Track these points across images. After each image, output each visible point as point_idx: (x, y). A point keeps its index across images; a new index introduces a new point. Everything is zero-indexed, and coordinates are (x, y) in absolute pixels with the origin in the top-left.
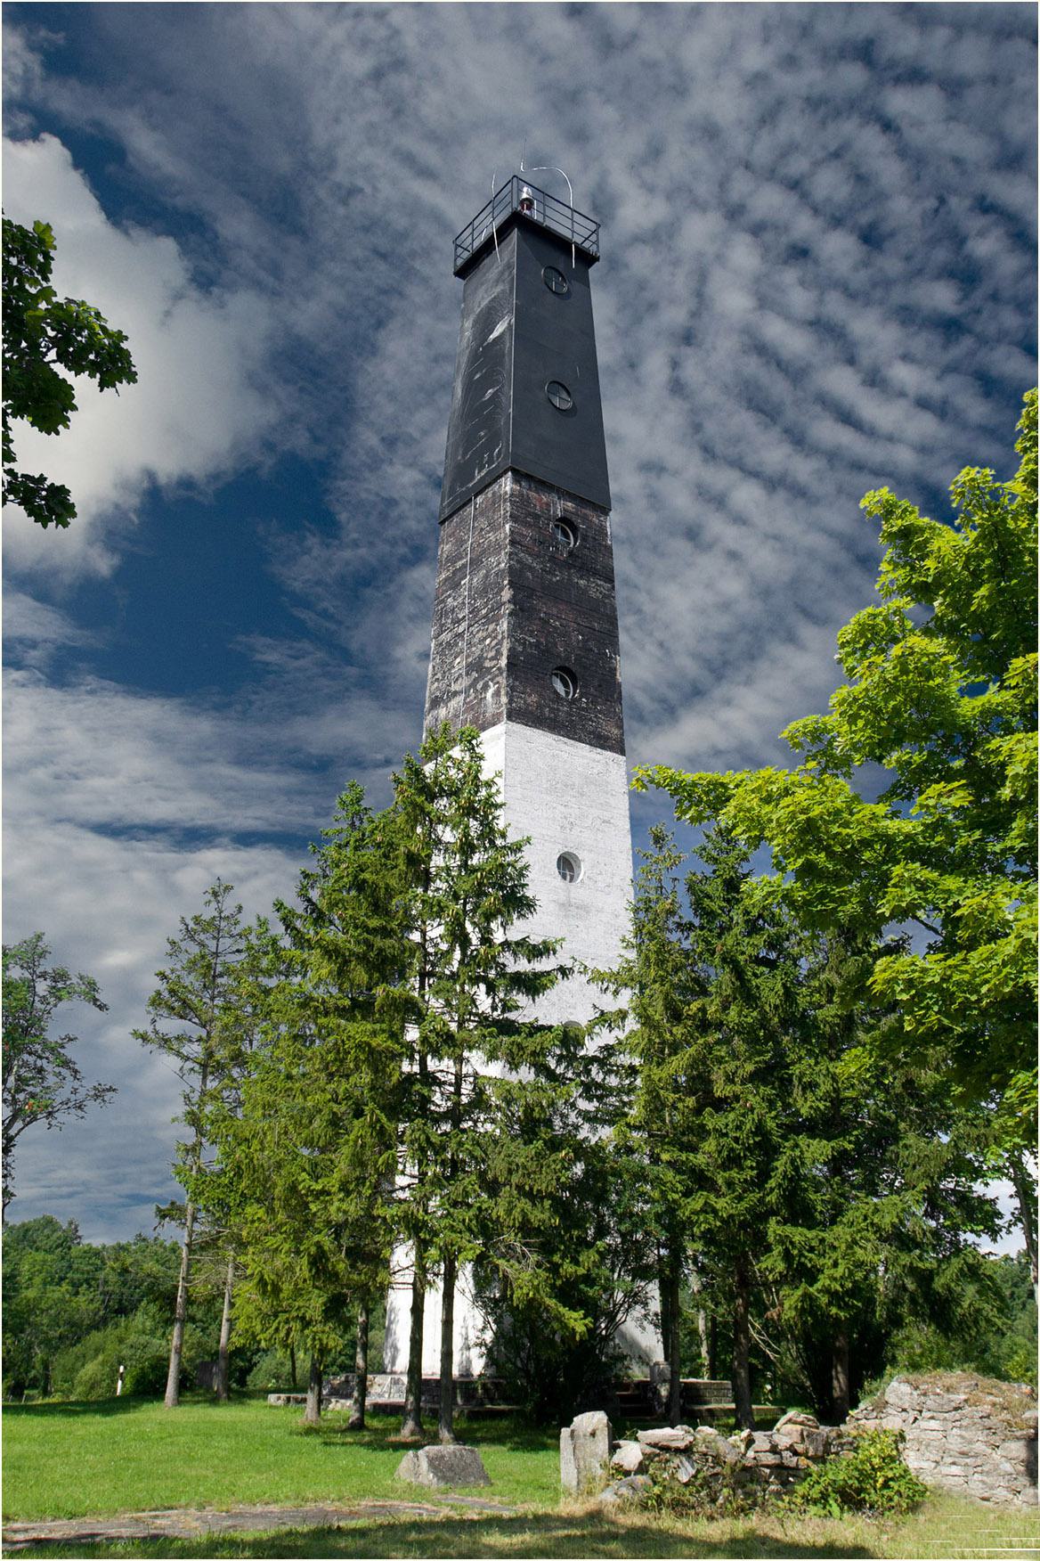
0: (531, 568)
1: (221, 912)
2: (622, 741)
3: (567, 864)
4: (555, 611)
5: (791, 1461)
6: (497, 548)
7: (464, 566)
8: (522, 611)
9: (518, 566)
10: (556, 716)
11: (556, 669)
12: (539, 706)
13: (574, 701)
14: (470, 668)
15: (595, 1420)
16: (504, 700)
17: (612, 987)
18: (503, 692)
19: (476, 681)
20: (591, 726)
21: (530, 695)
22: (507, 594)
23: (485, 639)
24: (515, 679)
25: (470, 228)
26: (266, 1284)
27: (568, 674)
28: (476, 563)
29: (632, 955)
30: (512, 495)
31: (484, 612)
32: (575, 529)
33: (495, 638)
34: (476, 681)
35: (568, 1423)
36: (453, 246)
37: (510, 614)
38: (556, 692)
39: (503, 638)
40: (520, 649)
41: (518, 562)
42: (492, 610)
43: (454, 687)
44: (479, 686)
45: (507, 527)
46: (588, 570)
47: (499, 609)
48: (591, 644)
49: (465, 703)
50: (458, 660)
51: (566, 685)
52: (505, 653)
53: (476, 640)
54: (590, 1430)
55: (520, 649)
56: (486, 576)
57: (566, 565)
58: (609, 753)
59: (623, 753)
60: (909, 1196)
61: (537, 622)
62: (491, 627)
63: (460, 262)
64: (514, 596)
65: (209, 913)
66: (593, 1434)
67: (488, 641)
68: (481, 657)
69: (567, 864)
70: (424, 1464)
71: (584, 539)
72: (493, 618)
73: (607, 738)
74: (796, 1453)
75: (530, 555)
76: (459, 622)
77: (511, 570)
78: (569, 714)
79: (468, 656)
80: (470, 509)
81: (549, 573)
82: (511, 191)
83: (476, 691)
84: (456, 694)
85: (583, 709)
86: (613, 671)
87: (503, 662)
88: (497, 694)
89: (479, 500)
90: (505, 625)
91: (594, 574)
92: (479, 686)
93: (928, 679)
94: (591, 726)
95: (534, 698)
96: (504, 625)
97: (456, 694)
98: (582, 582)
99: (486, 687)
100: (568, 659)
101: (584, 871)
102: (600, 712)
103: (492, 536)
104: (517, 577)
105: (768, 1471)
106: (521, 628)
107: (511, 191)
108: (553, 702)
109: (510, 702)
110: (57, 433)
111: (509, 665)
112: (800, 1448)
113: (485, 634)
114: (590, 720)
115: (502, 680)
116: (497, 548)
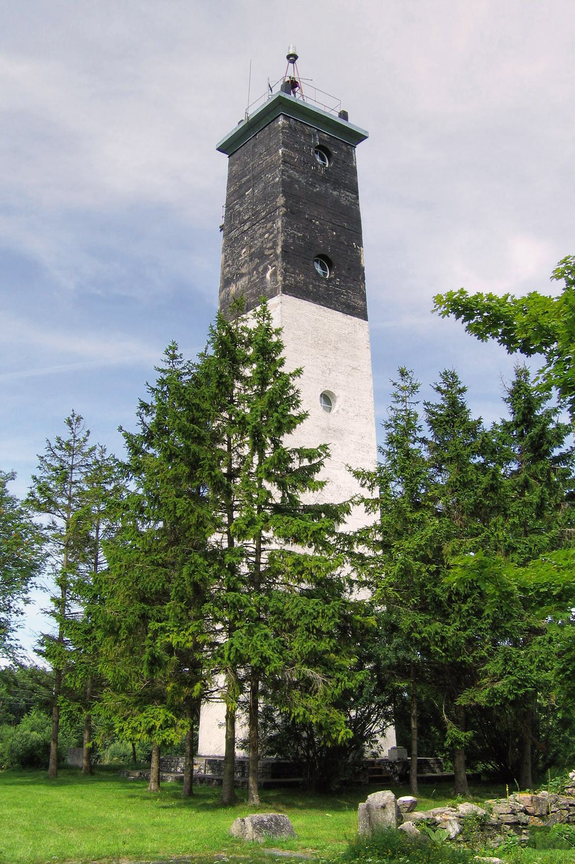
0: (298, 182)
1: (75, 437)
3: (327, 398)
4: (316, 213)
5: (523, 818)
6: (271, 167)
8: (292, 214)
10: (318, 291)
11: (316, 257)
12: (306, 284)
13: (330, 280)
14: (252, 256)
15: (385, 798)
16: (280, 278)
17: (369, 484)
18: (278, 273)
19: (258, 265)
20: (343, 298)
21: (299, 275)
22: (281, 200)
24: (287, 263)
27: (325, 260)
29: (383, 459)
30: (283, 128)
31: (263, 214)
32: (329, 155)
33: (272, 233)
34: (258, 265)
35: (364, 799)
37: (284, 215)
38: (317, 273)
39: (278, 232)
40: (291, 241)
41: (289, 177)
43: (243, 271)
44: (260, 269)
45: (280, 151)
46: (337, 184)
47: (275, 211)
48: (343, 238)
50: (244, 250)
51: (323, 268)
52: (280, 243)
54: (381, 804)
55: (291, 241)
56: (265, 188)
57: (324, 180)
60: (297, 666)
61: (303, 221)
62: (269, 225)
64: (286, 202)
65: (66, 437)
66: (384, 807)
67: (267, 235)
68: (261, 247)
69: (327, 398)
70: (249, 824)
71: (336, 162)
72: (270, 218)
73: (354, 308)
74: (526, 813)
75: (296, 171)
76: (245, 222)
77: (283, 183)
78: (327, 289)
79: (251, 247)
81: (311, 185)
83: (258, 273)
85: (337, 286)
86: (359, 259)
87: (279, 250)
88: (274, 274)
90: (280, 223)
91: (344, 188)
92: (260, 269)
94: (343, 298)
95: (302, 277)
96: (279, 223)
97: (242, 275)
98: (335, 193)
99: (266, 270)
101: (337, 406)
103: (268, 159)
104: (288, 188)
105: (509, 827)
106: (291, 225)
108: (315, 280)
109: (284, 280)
111: (285, 252)
112: (531, 809)
113: (264, 230)
114: (342, 294)
115: (279, 264)
116: (271, 167)
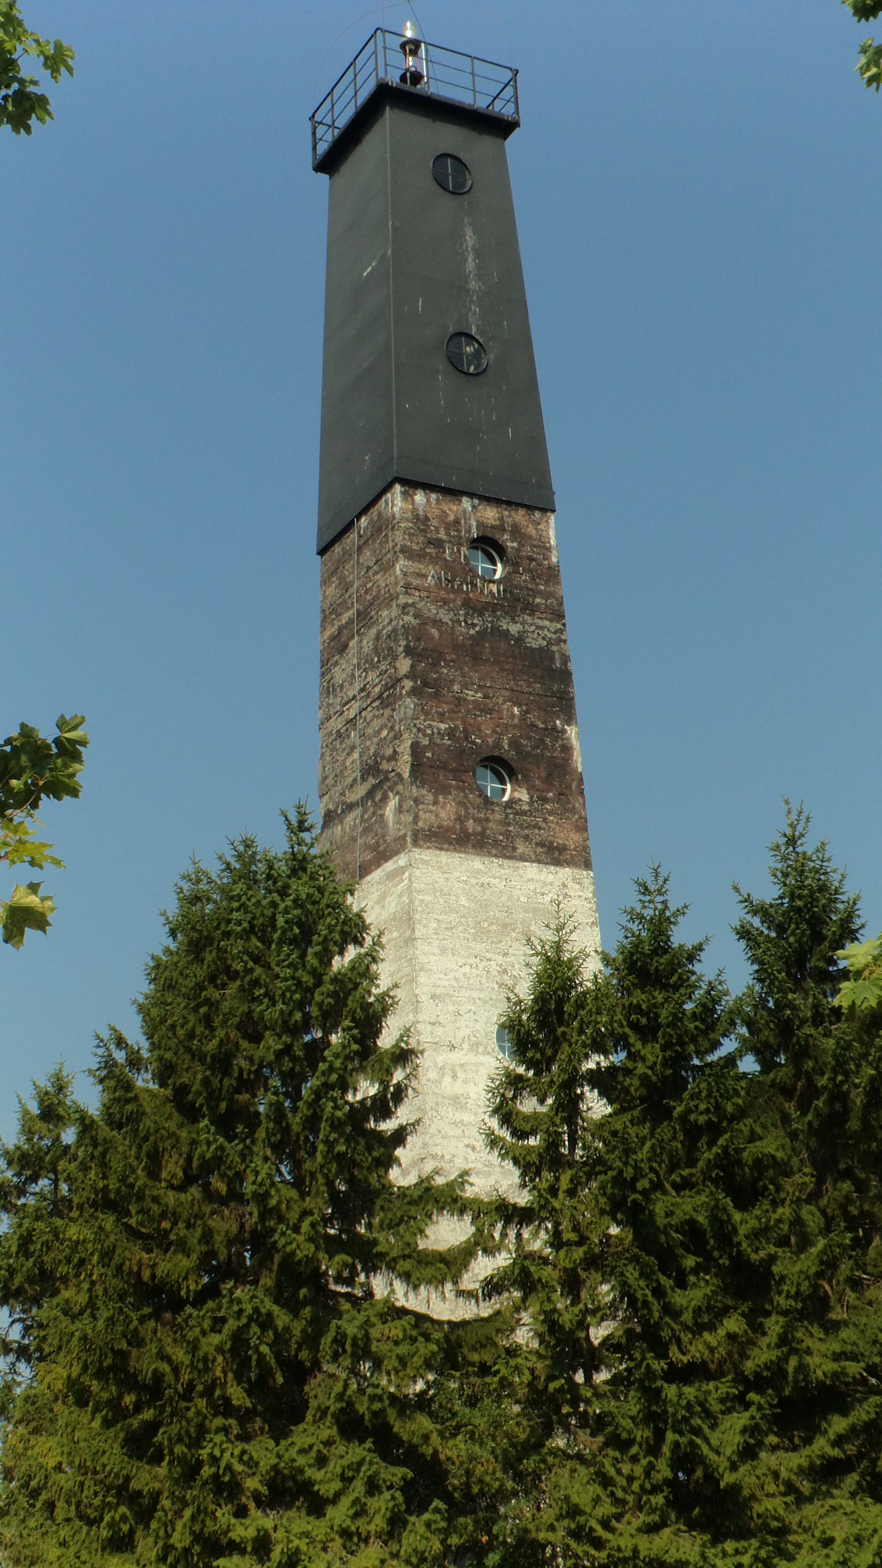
2: (585, 848)
7: (350, 621)
9: (414, 622)
10: (484, 829)
23: (381, 729)
25: (350, 75)
26: (625, 1037)
28: (364, 617)
32: (501, 551)
36: (309, 124)
42: (387, 688)
49: (363, 820)
53: (370, 731)
58: (567, 870)
59: (587, 865)
63: (323, 147)
73: (563, 849)
80: (352, 537)
82: (375, 52)
83: (375, 805)
84: (350, 807)
89: (364, 521)
93: (829, 965)
97: (350, 807)
100: (498, 745)
102: (550, 813)
107: (375, 52)
110: (28, 130)
